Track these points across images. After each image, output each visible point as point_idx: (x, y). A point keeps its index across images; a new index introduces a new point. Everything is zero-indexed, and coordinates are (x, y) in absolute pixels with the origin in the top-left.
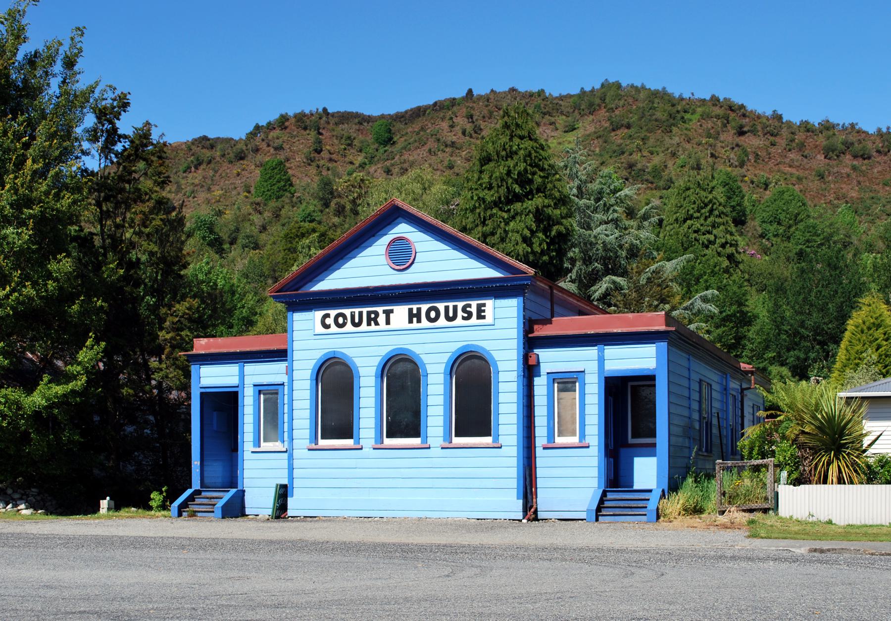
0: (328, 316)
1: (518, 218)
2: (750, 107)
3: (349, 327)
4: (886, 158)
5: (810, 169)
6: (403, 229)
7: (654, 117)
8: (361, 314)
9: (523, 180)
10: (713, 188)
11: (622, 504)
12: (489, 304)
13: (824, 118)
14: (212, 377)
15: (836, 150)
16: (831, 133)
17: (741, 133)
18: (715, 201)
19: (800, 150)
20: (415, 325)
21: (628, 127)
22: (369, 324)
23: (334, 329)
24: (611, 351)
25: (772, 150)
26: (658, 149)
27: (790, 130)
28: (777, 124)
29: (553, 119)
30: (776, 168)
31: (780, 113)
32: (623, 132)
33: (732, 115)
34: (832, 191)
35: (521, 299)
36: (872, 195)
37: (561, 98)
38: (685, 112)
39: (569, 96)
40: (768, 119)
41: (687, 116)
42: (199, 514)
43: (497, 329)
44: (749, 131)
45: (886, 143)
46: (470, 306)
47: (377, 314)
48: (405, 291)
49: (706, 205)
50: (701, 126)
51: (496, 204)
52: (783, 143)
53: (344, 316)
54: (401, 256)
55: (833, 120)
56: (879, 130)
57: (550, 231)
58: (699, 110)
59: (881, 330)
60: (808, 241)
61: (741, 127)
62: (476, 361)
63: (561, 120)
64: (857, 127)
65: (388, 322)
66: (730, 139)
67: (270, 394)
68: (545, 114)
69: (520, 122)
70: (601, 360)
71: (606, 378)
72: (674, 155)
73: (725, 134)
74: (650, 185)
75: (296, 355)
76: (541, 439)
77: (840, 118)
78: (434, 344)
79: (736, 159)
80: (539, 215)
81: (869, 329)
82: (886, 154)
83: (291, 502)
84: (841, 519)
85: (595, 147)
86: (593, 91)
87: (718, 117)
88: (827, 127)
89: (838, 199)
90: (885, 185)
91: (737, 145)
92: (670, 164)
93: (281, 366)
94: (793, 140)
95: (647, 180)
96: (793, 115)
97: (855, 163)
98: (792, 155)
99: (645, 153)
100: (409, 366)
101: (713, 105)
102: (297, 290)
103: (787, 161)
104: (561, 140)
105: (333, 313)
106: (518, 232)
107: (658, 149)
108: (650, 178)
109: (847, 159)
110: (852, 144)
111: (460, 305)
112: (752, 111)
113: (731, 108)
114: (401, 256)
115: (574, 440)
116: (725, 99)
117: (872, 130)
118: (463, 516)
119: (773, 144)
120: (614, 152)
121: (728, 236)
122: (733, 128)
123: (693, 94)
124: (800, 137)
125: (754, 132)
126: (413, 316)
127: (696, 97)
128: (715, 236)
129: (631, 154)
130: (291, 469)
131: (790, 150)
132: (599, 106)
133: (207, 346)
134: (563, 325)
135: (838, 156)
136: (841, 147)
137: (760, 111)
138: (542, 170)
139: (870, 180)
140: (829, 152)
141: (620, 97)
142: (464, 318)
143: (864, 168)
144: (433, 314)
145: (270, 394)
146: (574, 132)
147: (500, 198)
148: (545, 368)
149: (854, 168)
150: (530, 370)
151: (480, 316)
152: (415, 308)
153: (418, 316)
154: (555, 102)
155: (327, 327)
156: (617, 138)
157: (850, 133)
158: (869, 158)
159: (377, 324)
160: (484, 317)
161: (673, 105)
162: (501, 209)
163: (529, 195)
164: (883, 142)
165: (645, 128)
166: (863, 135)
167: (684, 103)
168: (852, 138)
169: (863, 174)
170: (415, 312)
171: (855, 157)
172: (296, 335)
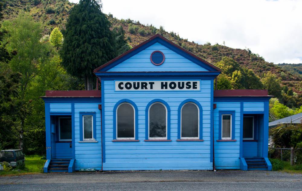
0: (122, 83)
20: (144, 90)
23: (125, 89)
126: (163, 86)
153: (166, 86)
159: (146, 88)
160: (196, 88)
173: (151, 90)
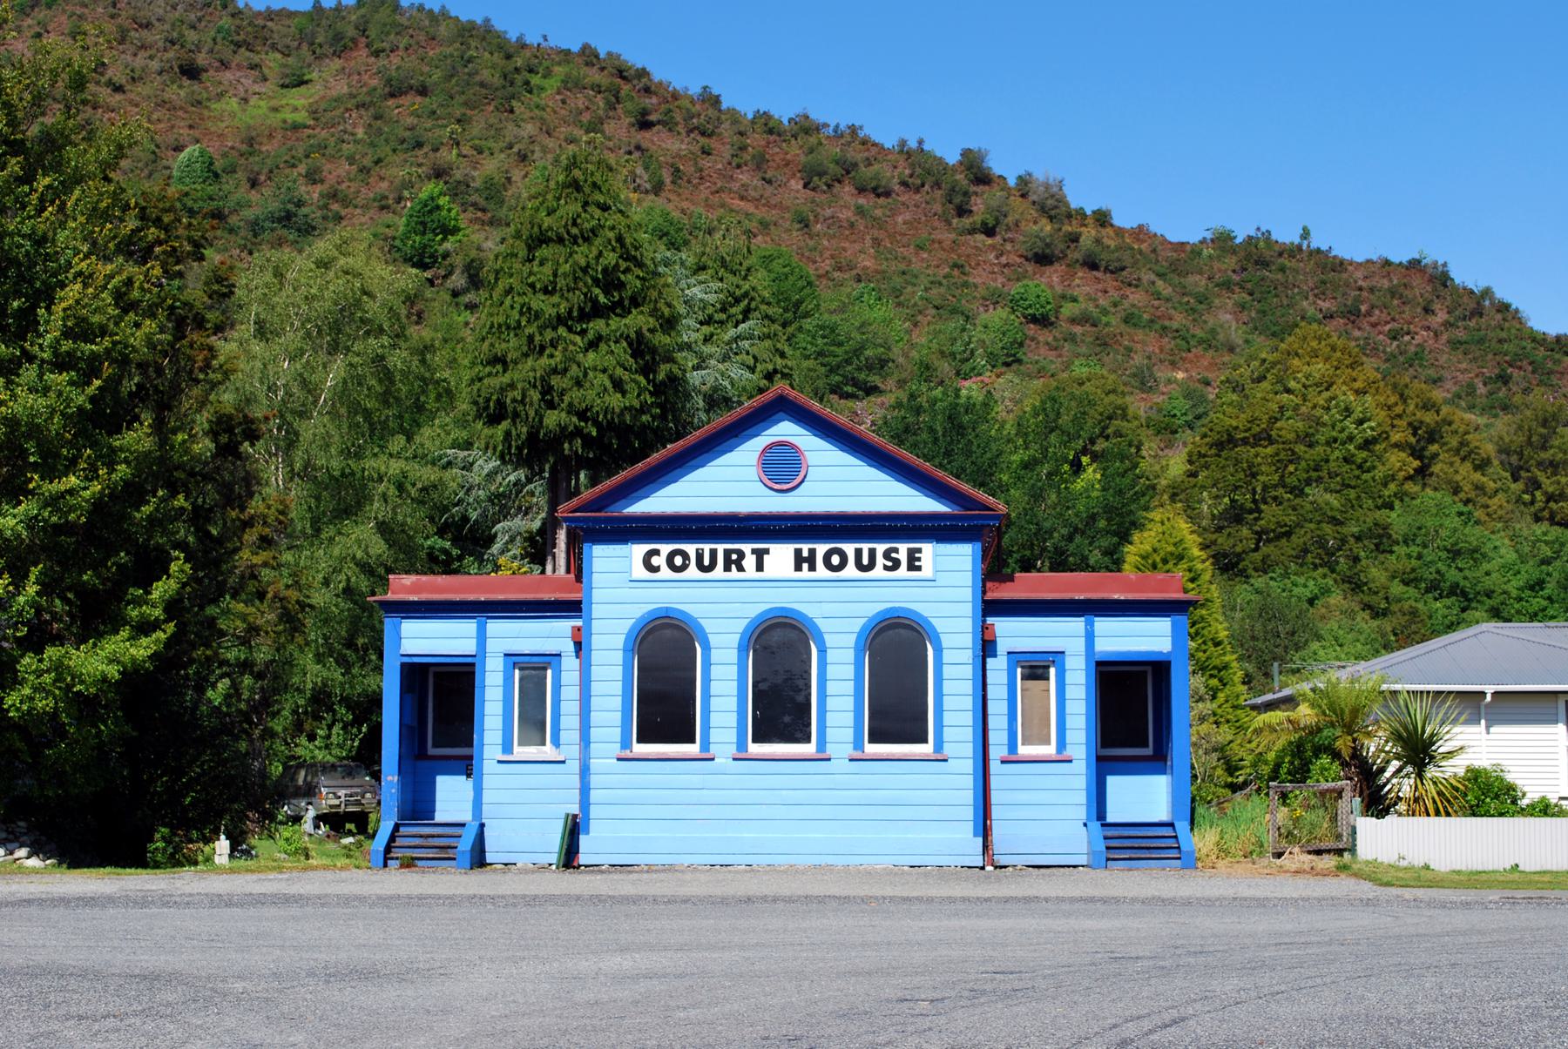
0: (656, 552)
1: (603, 347)
2: (658, 75)
3: (693, 571)
4: (917, 197)
5: (780, 206)
6: (786, 430)
7: (478, 78)
8: (713, 553)
9: (610, 281)
10: (748, 270)
11: (1136, 843)
12: (928, 550)
13: (800, 111)
14: (422, 638)
15: (825, 173)
16: (813, 140)
17: (645, 125)
18: (752, 294)
19: (759, 168)
20: (805, 573)
21: (423, 91)
22: (727, 568)
23: (665, 572)
24: (1103, 625)
25: (705, 163)
26: (491, 143)
27: (736, 128)
28: (711, 112)
29: (256, 59)
30: (716, 199)
31: (715, 92)
32: (412, 101)
33: (626, 88)
34: (827, 254)
35: (978, 545)
36: (902, 267)
37: (270, 15)
38: (531, 71)
39: (291, 15)
40: (692, 102)
41: (535, 80)
42: (419, 863)
43: (944, 582)
44: (659, 122)
45: (919, 171)
46: (896, 550)
47: (741, 555)
48: (797, 523)
49: (737, 301)
50: (564, 102)
51: (561, 320)
52: (727, 152)
53: (685, 556)
54: (782, 468)
55: (817, 116)
56: (903, 143)
57: (655, 372)
58: (559, 70)
59: (1184, 565)
60: (821, 354)
61: (644, 112)
62: (902, 631)
63: (272, 62)
64: (861, 134)
65: (760, 567)
66: (623, 133)
67: (533, 671)
68: (238, 45)
69: (598, 178)
70: (1090, 637)
71: (1099, 664)
72: (523, 158)
73: (612, 122)
74: (479, 214)
75: (597, 610)
76: (997, 751)
77: (832, 113)
78: (840, 604)
79: (646, 177)
80: (639, 346)
81: (1165, 561)
82: (917, 191)
83: (584, 841)
84: (1443, 863)
85: (355, 125)
86: (338, 9)
87: (598, 89)
88: (805, 127)
89: (840, 269)
90: (920, 248)
91: (638, 148)
92: (516, 175)
93: (564, 626)
94: (743, 148)
95: (474, 205)
96: (742, 99)
97: (862, 201)
98: (743, 177)
99: (466, 150)
100: (793, 635)
101: (587, 64)
102: (599, 510)
103: (735, 186)
104: (274, 103)
105: (665, 549)
106: (604, 371)
107: (491, 143)
108: (482, 202)
109: (846, 190)
110: (855, 165)
111: (881, 548)
112: (661, 83)
113: (621, 73)
114: (782, 468)
115: (1050, 750)
116: (610, 54)
117: (889, 142)
118: (886, 862)
119: (706, 152)
120: (403, 141)
121: (779, 361)
122: (628, 113)
123: (545, 38)
124: (756, 140)
125: (668, 124)
127: (552, 43)
128: (755, 357)
129: (436, 150)
130: (585, 790)
131: (739, 166)
132: (354, 40)
133: (414, 589)
134: (1025, 586)
135: (829, 186)
136: (834, 169)
137: (677, 84)
138: (640, 265)
139: (891, 236)
140: (812, 176)
141: (400, 30)
142: (886, 568)
143: (878, 212)
144: (835, 560)
145: (533, 671)
146: (303, 89)
147: (570, 311)
148: (1003, 646)
149: (860, 211)
150: (987, 647)
151: (913, 566)
152: (805, 548)
154: (260, 22)
155: (656, 569)
156: (404, 110)
157: (849, 144)
158: (887, 194)
159: (741, 569)
160: (919, 568)
161: (508, 57)
162: (570, 330)
163: (618, 309)
164: (912, 166)
165: (460, 99)
166: (874, 150)
167: (527, 53)
168: (856, 154)
169: (878, 223)
170: (805, 554)
171: (861, 190)
172: (597, 579)
173: (759, 575)
